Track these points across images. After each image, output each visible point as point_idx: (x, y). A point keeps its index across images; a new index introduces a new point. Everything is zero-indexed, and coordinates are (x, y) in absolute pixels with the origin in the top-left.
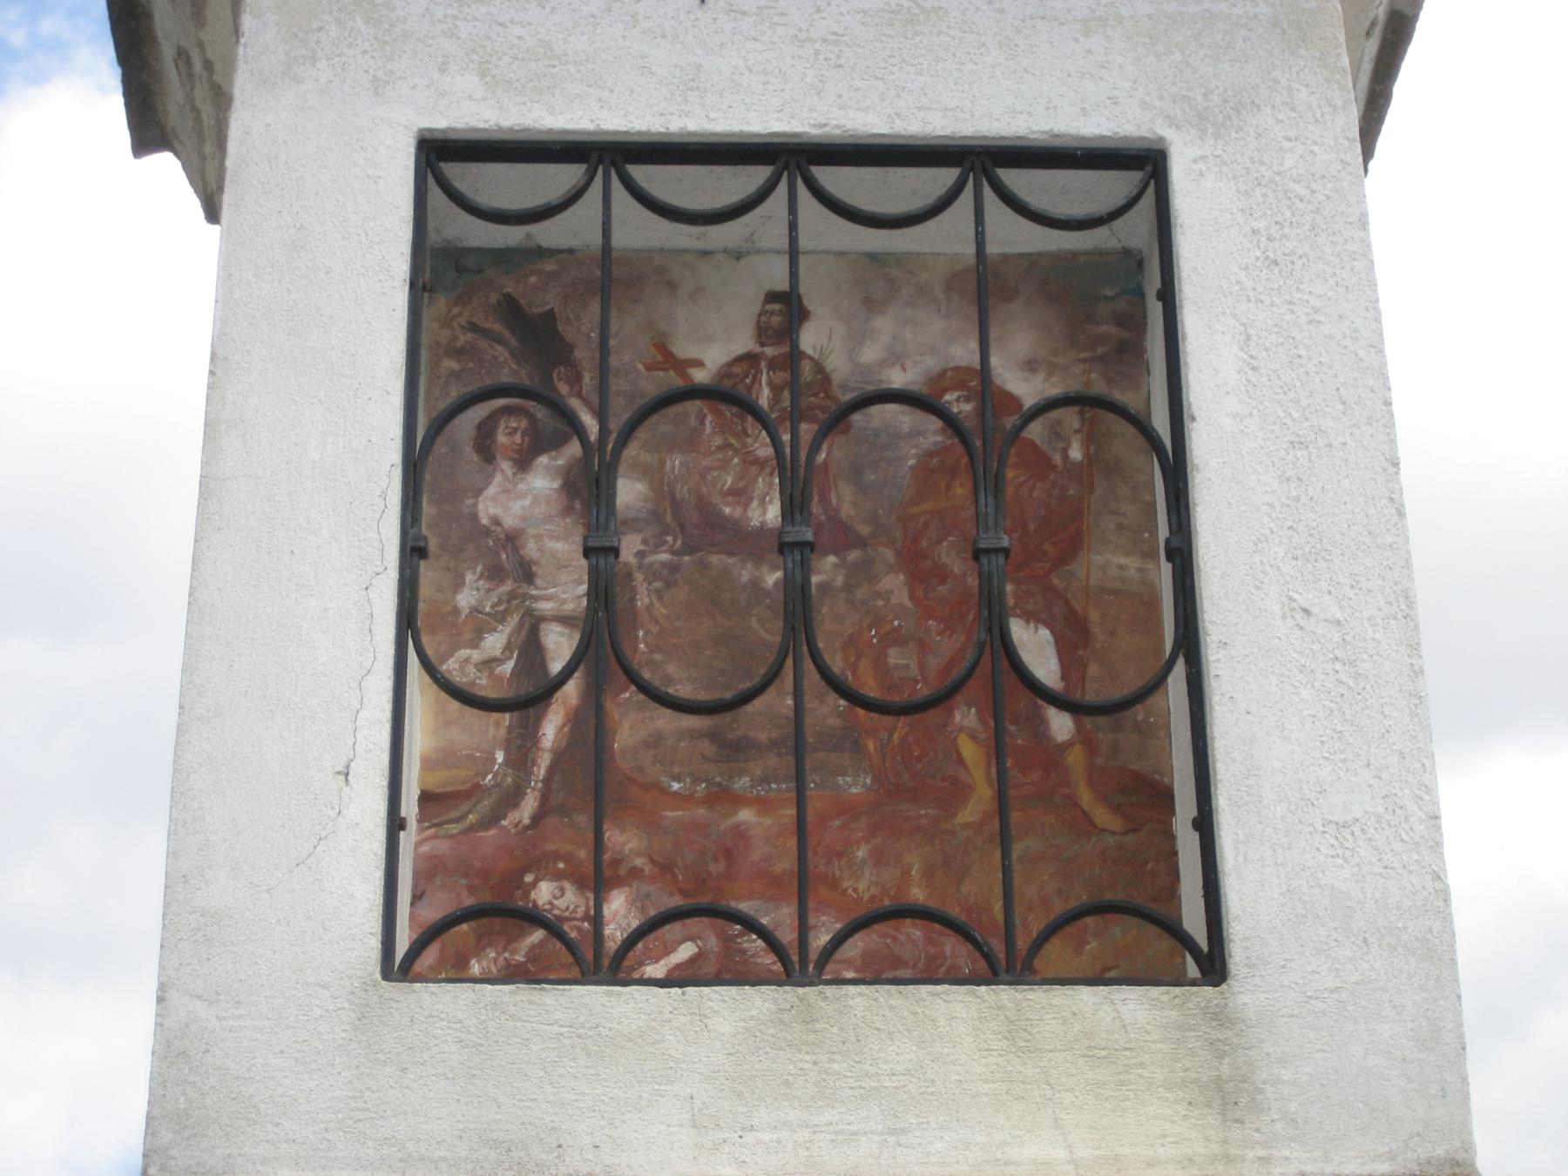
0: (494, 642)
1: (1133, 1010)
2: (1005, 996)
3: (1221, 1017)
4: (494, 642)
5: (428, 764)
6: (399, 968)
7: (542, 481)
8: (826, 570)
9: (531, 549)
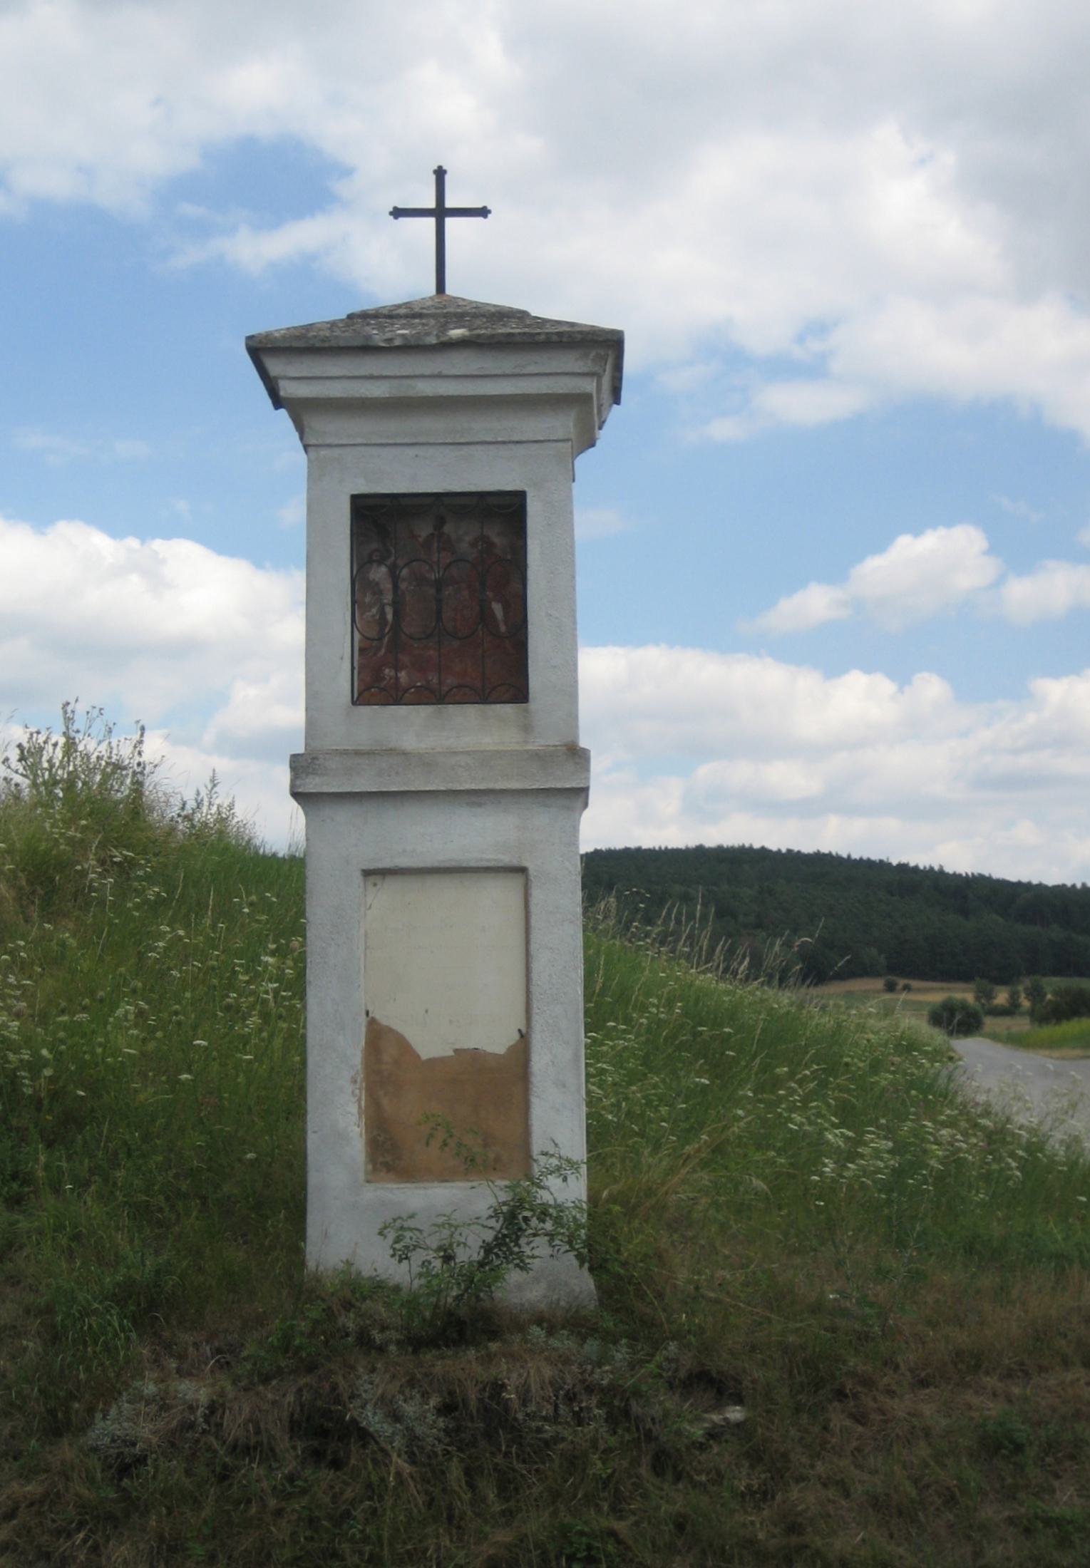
0: (374, 611)
1: (508, 710)
2: (481, 707)
3: (526, 710)
4: (374, 611)
5: (360, 641)
6: (355, 702)
7: (383, 569)
8: (448, 591)
9: (382, 586)
